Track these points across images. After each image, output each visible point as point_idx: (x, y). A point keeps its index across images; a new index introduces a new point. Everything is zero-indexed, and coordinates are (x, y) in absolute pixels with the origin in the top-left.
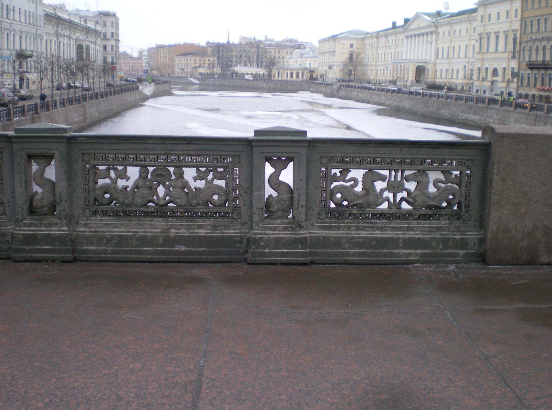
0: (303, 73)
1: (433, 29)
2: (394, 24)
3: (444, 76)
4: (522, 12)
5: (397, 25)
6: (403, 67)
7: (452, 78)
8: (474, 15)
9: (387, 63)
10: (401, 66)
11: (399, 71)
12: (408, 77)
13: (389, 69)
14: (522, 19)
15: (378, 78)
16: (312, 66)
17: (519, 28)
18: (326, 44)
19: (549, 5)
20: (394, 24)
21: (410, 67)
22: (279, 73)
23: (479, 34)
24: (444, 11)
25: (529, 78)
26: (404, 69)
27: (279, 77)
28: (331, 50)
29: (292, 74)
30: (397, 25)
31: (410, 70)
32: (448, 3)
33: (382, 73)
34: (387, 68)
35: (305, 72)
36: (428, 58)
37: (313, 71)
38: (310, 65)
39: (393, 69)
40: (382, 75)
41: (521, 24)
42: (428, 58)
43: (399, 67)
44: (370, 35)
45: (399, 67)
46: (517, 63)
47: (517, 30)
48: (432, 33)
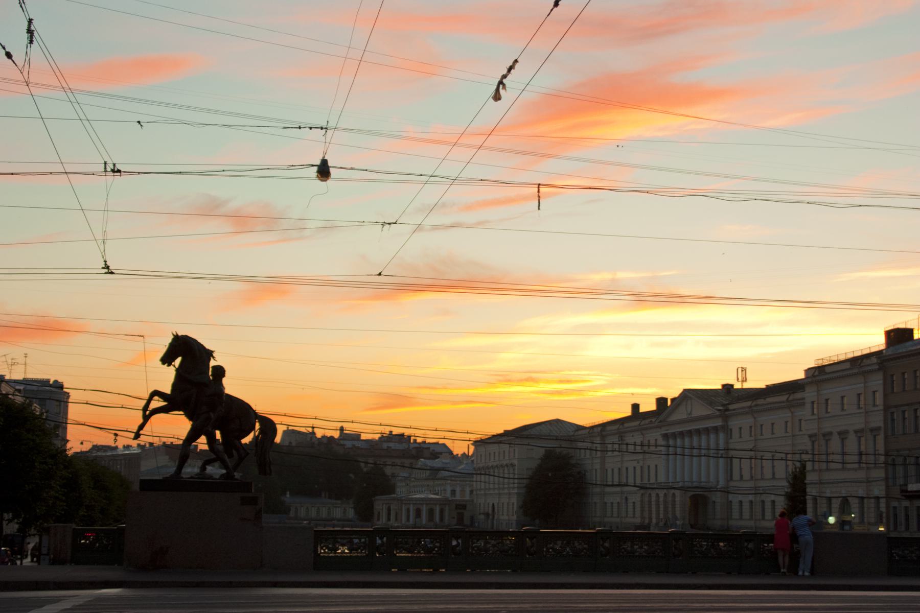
0: (442, 511)
1: (719, 423)
2: (635, 407)
3: (746, 515)
4: (885, 395)
5: (642, 409)
6: (661, 499)
7: (763, 518)
8: (798, 395)
9: (762, 484)
10: (657, 495)
11: (654, 509)
12: (650, 519)
13: (630, 501)
14: (887, 407)
15: (606, 520)
16: (458, 497)
17: (881, 424)
18: (493, 448)
19: (918, 387)
20: (635, 407)
21: (678, 499)
22: (389, 510)
23: (810, 436)
24: (738, 386)
25: (907, 516)
26: (665, 502)
27: (389, 519)
28: (505, 463)
29: (418, 513)
30: (642, 409)
31: (678, 503)
32: (744, 370)
33: (615, 510)
34: (626, 499)
35: (447, 508)
36: (712, 479)
37: (464, 507)
38: (453, 492)
39: (642, 501)
40: (615, 515)
41: (885, 416)
42: (712, 479)
43: (654, 499)
44: (586, 431)
45: (654, 499)
46: (884, 487)
47: (879, 429)
48: (716, 429)
